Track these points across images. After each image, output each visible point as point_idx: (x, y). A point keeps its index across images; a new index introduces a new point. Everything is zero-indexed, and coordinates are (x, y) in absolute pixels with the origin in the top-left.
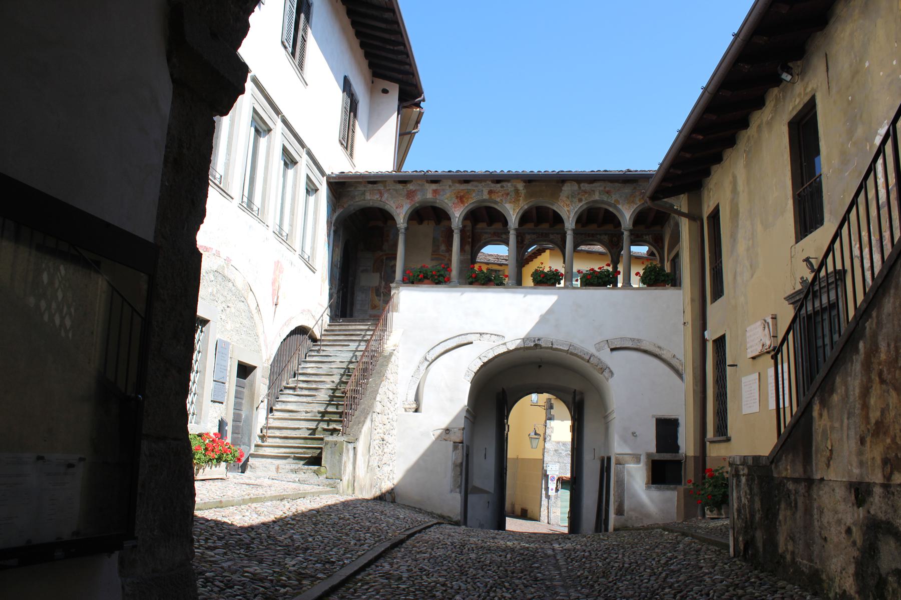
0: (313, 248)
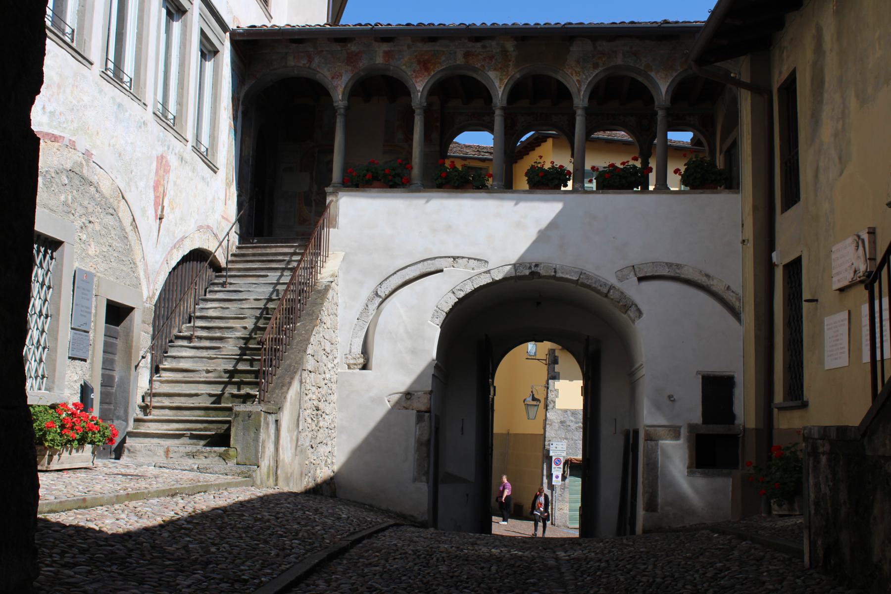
0: (213, 138)
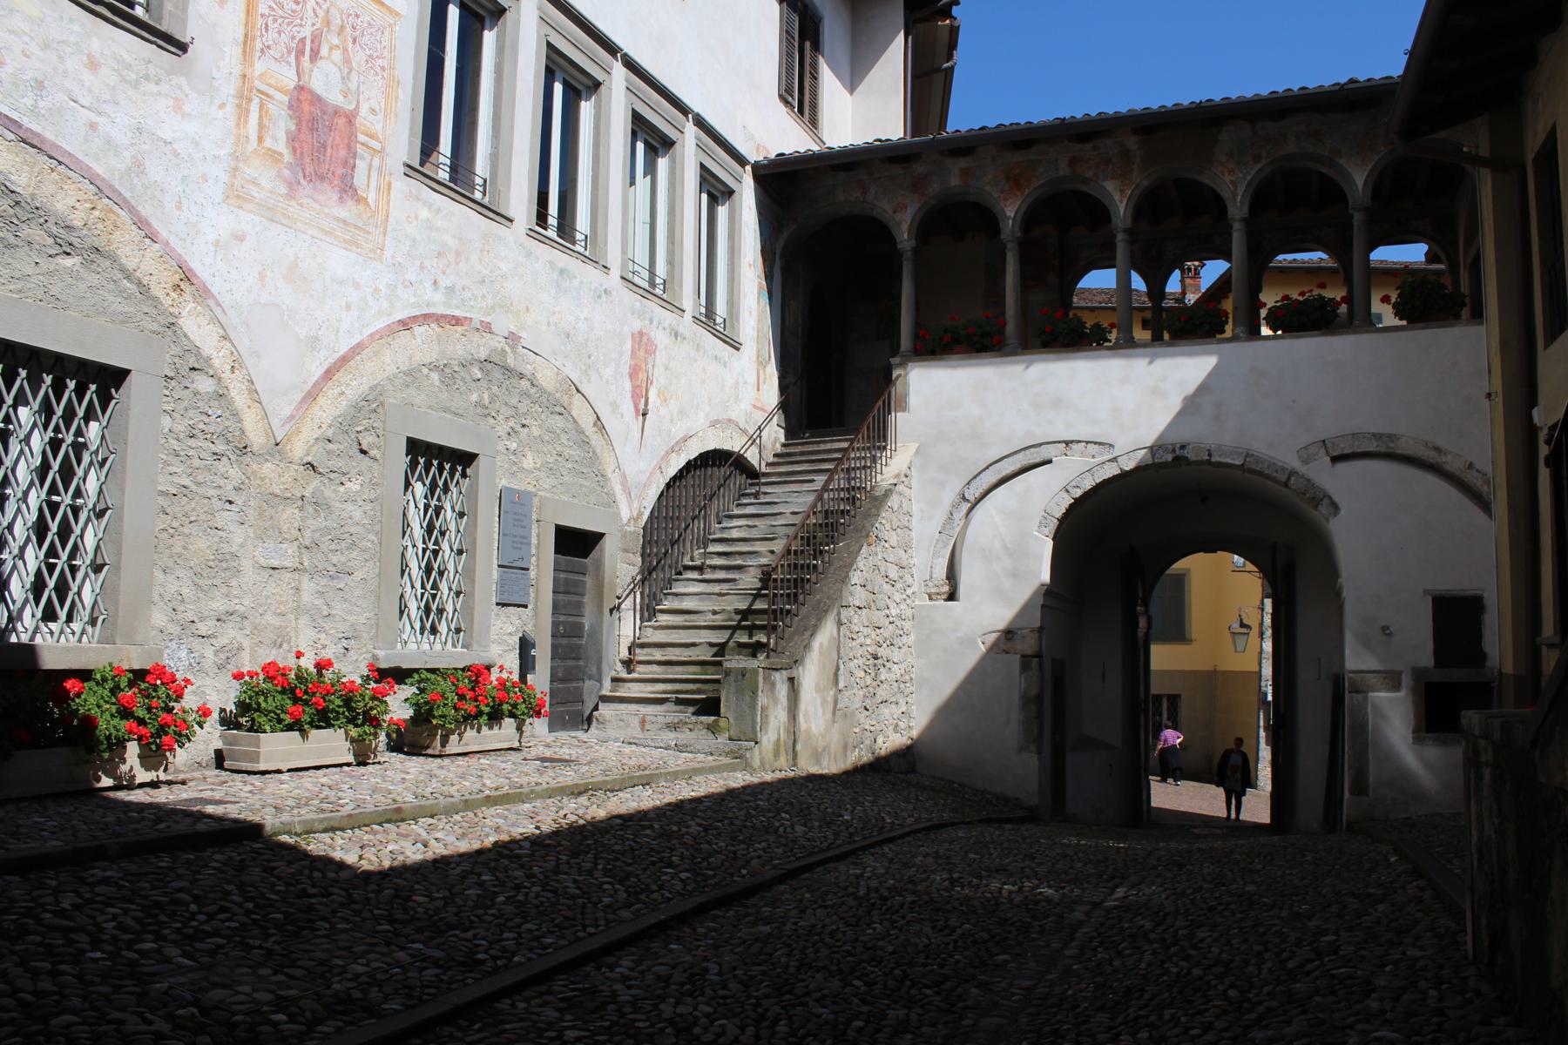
0: (732, 304)
